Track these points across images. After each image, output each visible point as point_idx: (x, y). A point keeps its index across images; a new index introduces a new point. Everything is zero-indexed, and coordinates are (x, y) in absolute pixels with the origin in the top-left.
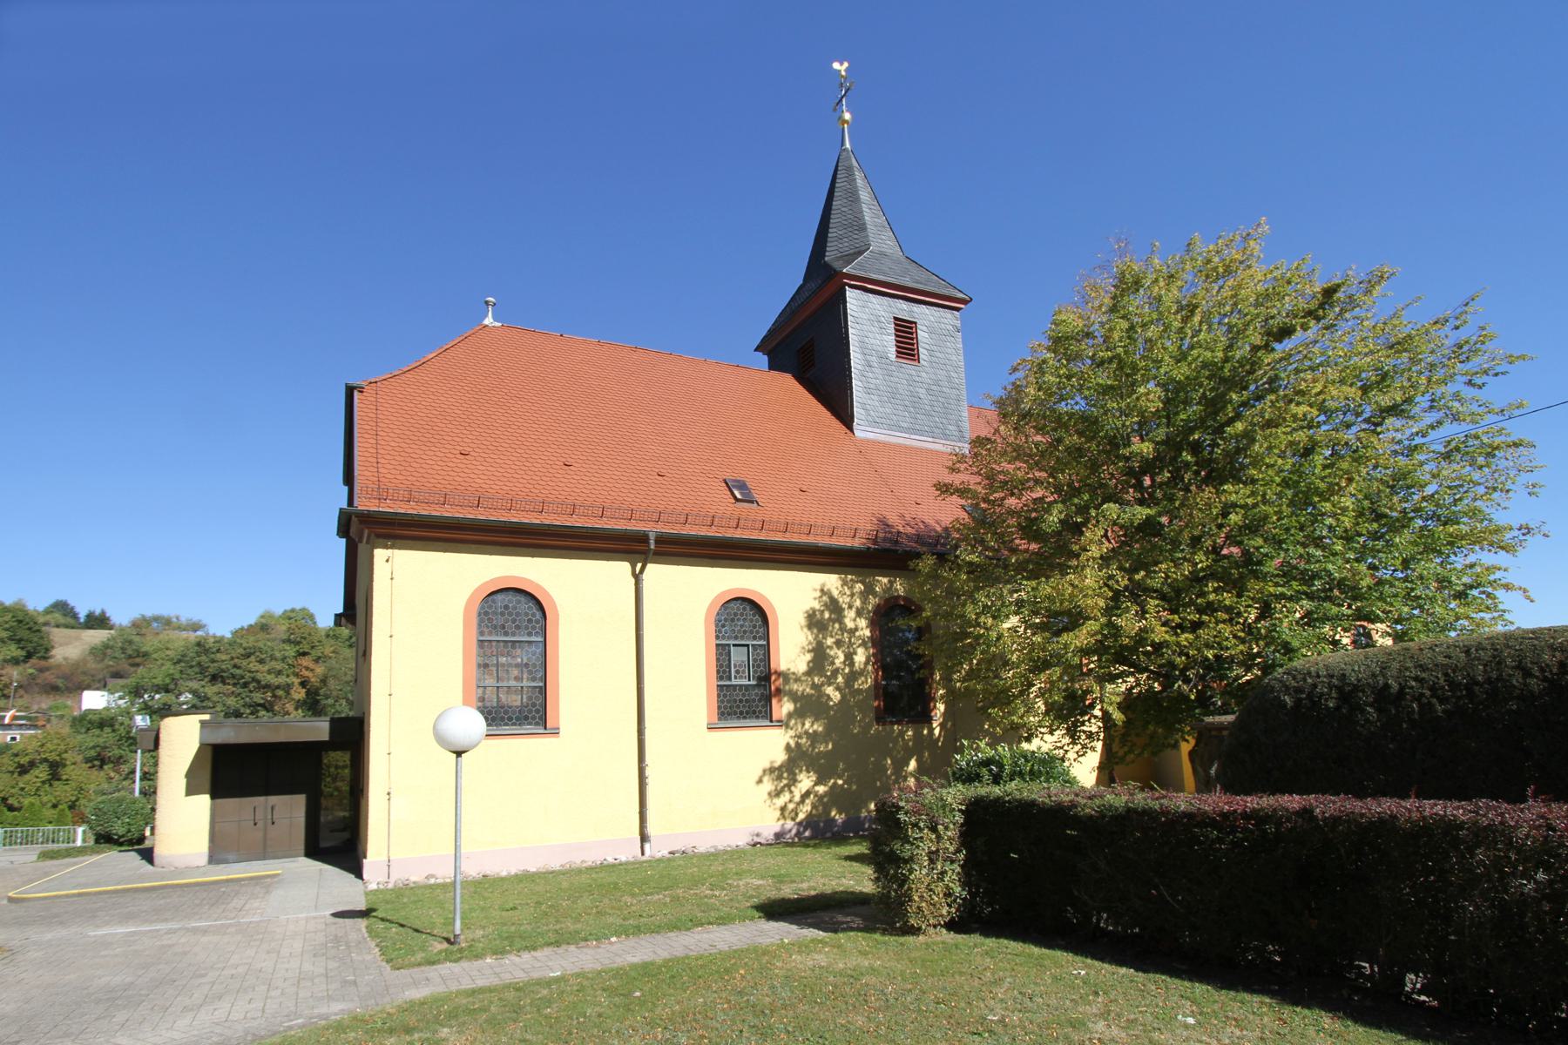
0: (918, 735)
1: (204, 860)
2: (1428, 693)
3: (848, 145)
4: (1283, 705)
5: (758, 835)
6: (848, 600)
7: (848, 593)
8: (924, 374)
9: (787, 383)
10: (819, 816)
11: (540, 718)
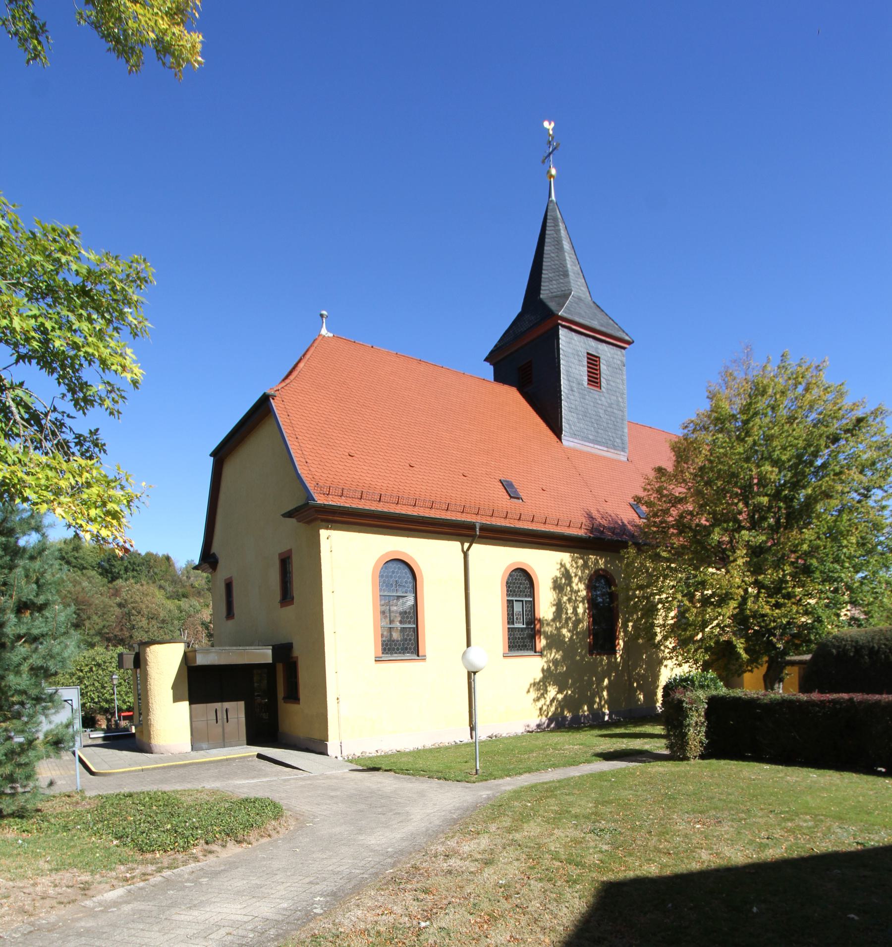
0: (609, 662)
1: (188, 748)
2: (888, 651)
3: (553, 197)
4: (832, 653)
5: (528, 726)
6: (575, 571)
7: (575, 566)
8: (603, 399)
9: (511, 395)
10: (559, 714)
11: (415, 649)
